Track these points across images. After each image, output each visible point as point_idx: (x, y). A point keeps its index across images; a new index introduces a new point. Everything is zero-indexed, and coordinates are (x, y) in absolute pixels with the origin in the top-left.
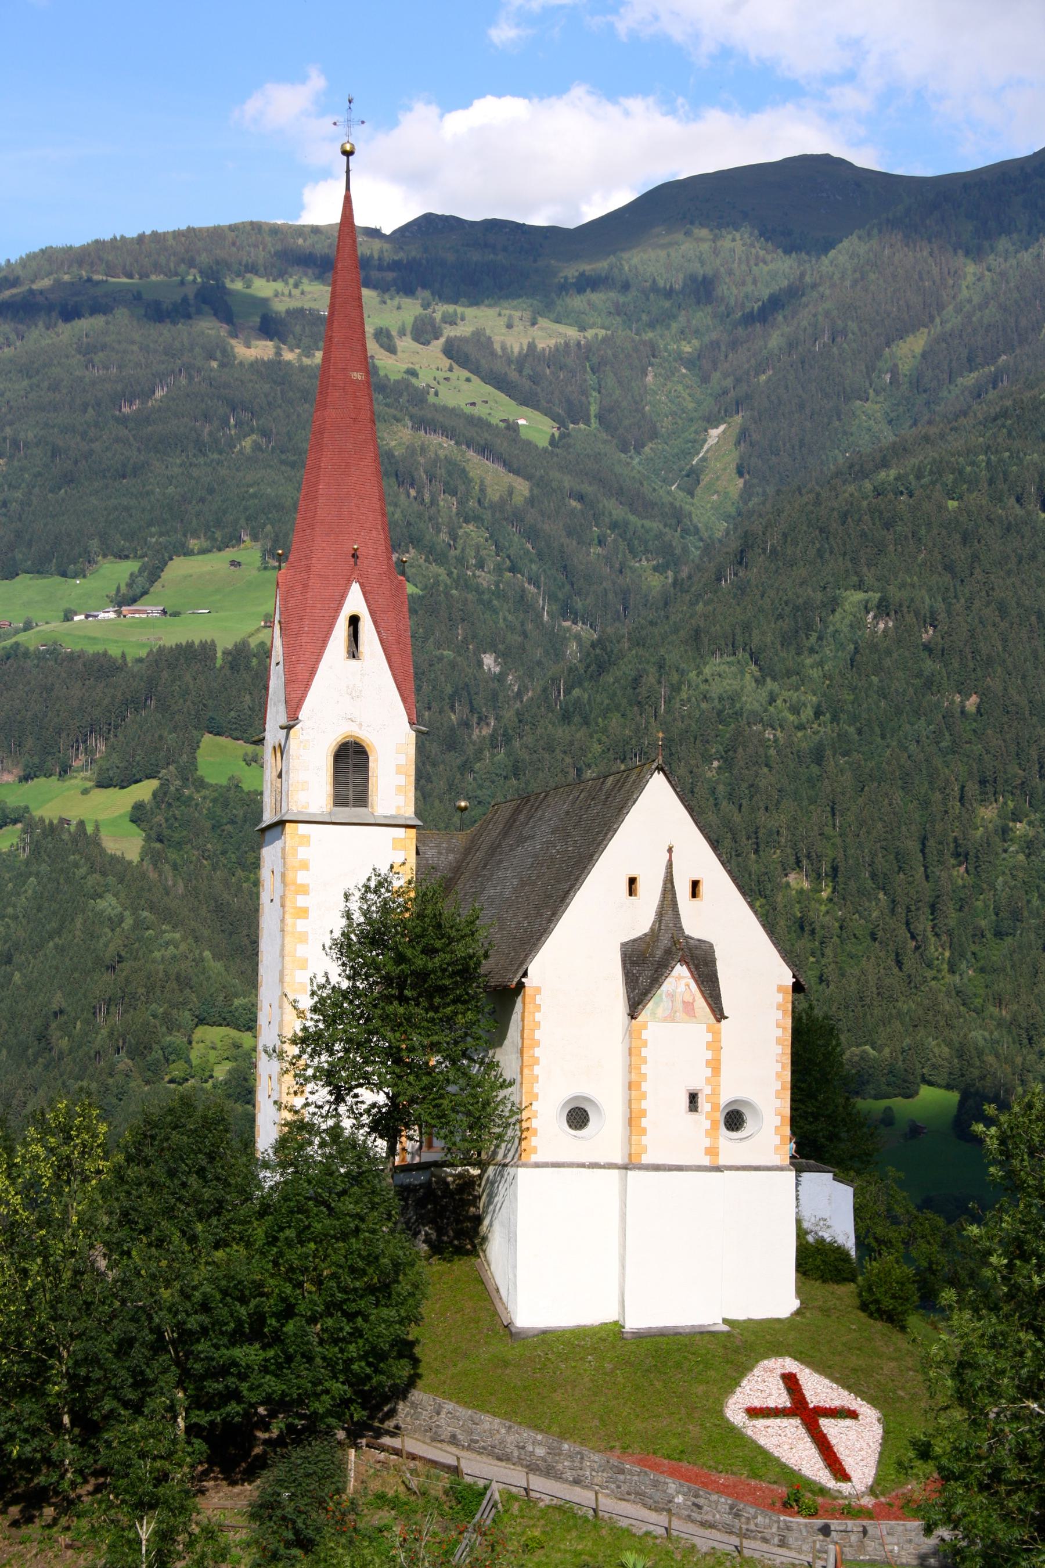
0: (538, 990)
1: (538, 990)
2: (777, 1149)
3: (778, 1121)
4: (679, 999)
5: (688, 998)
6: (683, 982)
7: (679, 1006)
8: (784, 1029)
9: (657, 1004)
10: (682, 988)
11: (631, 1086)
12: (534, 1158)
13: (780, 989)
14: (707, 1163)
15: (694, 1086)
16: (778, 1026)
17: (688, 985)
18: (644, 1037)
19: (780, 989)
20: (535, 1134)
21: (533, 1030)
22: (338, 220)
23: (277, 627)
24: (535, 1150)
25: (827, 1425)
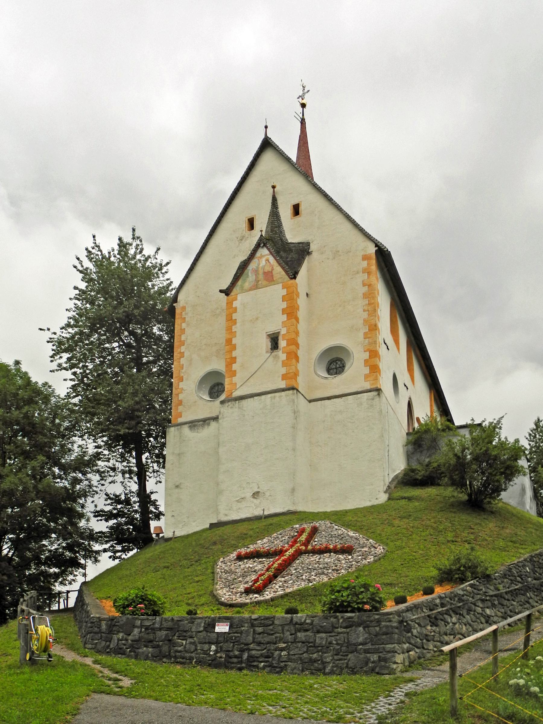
4: (261, 272)
6: (264, 260)
7: (261, 276)
10: (263, 262)
15: (272, 329)
17: (267, 260)
25: (318, 542)
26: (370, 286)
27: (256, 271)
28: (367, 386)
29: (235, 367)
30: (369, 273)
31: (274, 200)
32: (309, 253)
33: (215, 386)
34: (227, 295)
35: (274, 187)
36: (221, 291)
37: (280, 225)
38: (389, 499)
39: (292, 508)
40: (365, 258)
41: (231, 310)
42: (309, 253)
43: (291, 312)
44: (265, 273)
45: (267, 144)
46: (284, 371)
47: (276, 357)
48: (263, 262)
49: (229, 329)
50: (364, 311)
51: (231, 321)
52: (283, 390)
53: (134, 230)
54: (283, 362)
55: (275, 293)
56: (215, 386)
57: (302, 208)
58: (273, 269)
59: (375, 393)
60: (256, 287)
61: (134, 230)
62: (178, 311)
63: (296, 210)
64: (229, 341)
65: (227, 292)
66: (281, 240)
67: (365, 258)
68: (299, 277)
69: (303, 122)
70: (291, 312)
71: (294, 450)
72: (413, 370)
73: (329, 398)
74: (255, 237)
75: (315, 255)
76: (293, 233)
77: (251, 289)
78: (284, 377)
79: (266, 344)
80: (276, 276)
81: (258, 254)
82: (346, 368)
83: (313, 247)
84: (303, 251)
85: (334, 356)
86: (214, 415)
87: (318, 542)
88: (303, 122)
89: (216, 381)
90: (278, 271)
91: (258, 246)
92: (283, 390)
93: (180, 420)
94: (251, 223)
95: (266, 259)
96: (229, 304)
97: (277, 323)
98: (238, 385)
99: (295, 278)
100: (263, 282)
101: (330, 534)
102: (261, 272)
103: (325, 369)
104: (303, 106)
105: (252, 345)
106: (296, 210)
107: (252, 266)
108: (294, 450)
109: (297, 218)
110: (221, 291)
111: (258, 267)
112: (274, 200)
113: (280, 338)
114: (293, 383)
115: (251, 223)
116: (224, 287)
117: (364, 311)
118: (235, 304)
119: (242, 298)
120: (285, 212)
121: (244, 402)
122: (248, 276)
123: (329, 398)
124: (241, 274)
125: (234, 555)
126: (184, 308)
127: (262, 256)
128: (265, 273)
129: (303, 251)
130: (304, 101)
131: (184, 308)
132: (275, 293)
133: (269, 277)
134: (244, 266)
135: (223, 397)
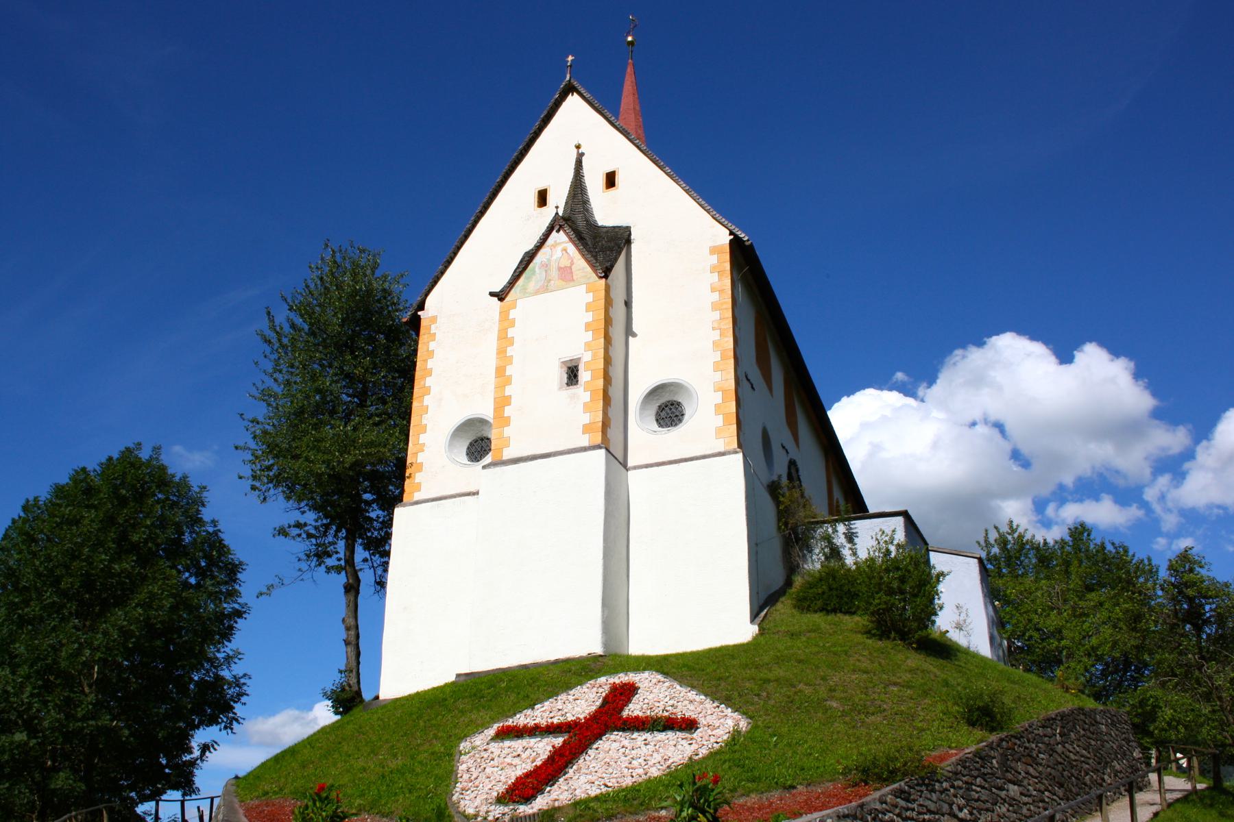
0: (434, 319)
1: (434, 319)
2: (719, 432)
3: (718, 397)
4: (554, 266)
5: (565, 263)
6: (559, 249)
7: (554, 273)
8: (721, 291)
9: (529, 278)
10: (558, 253)
11: (500, 371)
12: (417, 496)
13: (714, 250)
14: (586, 444)
15: (569, 354)
16: (713, 290)
17: (565, 250)
18: (511, 317)
19: (714, 250)
20: (420, 470)
21: (426, 361)
22: (829, 413)
23: (864, 800)
24: (418, 487)
25: (634, 709)
27: (546, 266)
29: (508, 411)
33: (478, 444)
34: (501, 299)
36: (492, 294)
37: (585, 202)
44: (560, 269)
48: (558, 253)
49: (501, 352)
50: (714, 329)
51: (504, 340)
54: (585, 405)
56: (478, 444)
58: (572, 263)
60: (545, 289)
62: (423, 323)
63: (611, 180)
65: (500, 296)
66: (587, 221)
72: (796, 423)
74: (548, 214)
76: (606, 210)
77: (537, 293)
80: (577, 274)
82: (686, 417)
85: (666, 398)
86: (473, 490)
87: (634, 709)
89: (479, 435)
90: (581, 265)
91: (550, 230)
94: (542, 198)
95: (562, 246)
96: (506, 322)
98: (514, 439)
100: (556, 282)
101: (655, 694)
102: (554, 266)
103: (654, 418)
105: (537, 375)
106: (611, 180)
109: (612, 191)
110: (492, 294)
111: (549, 260)
113: (581, 368)
115: (542, 198)
116: (497, 289)
117: (714, 329)
118: (513, 314)
119: (523, 303)
122: (534, 272)
124: (525, 269)
125: (491, 732)
128: (560, 269)
133: (566, 274)
134: (529, 257)
135: (488, 459)
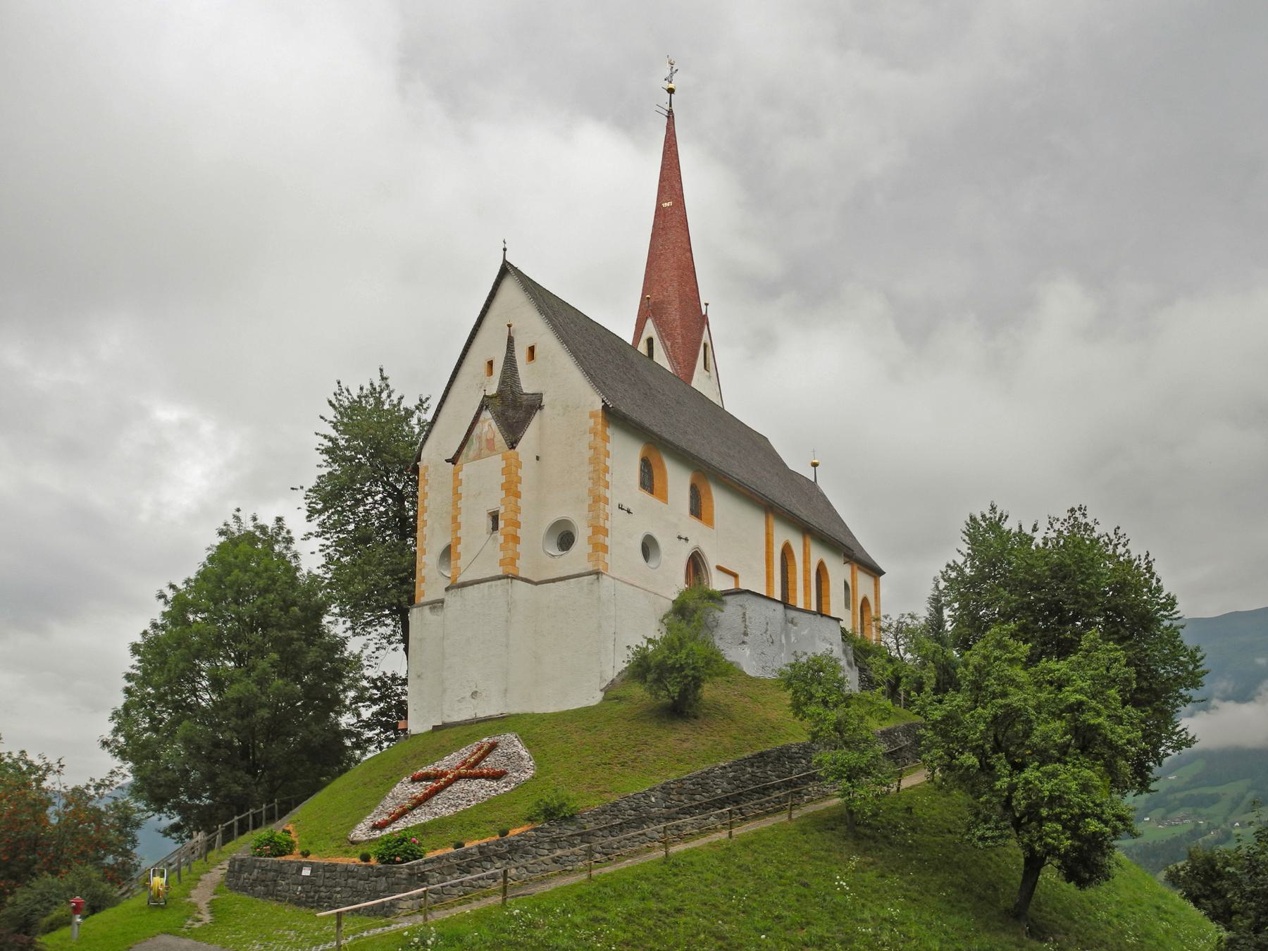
4: (484, 439)
7: (484, 444)
10: (486, 428)
26: (595, 449)
28: (590, 567)
30: (595, 434)
31: (511, 340)
32: (541, 407)
35: (509, 326)
38: (604, 699)
39: (506, 711)
40: (593, 415)
41: (457, 482)
42: (541, 407)
43: (511, 488)
45: (506, 270)
46: (501, 555)
47: (495, 539)
49: (455, 504)
52: (499, 578)
53: (381, 370)
55: (495, 463)
57: (536, 351)
59: (594, 577)
60: (479, 457)
61: (381, 370)
64: (455, 519)
65: (454, 461)
67: (593, 415)
68: (519, 447)
69: (670, 115)
70: (511, 488)
71: (507, 646)
73: (554, 581)
75: (546, 409)
77: (474, 459)
78: (502, 563)
79: (486, 522)
81: (482, 418)
83: (545, 400)
84: (535, 404)
88: (670, 115)
90: (499, 439)
92: (499, 578)
93: (423, 600)
96: (456, 474)
97: (495, 500)
99: (513, 448)
100: (485, 451)
104: (671, 91)
107: (476, 431)
108: (507, 646)
109: (533, 364)
112: (511, 340)
114: (511, 571)
119: (468, 468)
120: (521, 355)
121: (466, 590)
123: (554, 581)
126: (427, 468)
127: (486, 420)
129: (535, 404)
130: (671, 86)
131: (427, 468)
132: (495, 463)
